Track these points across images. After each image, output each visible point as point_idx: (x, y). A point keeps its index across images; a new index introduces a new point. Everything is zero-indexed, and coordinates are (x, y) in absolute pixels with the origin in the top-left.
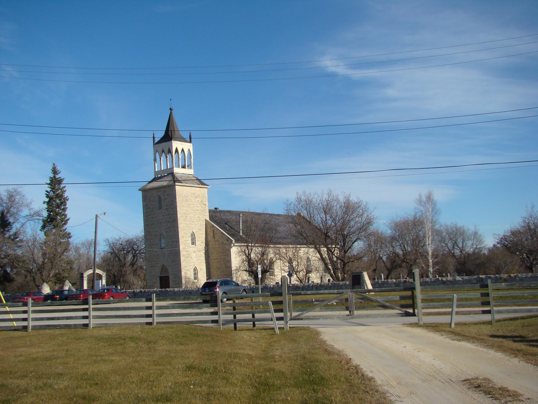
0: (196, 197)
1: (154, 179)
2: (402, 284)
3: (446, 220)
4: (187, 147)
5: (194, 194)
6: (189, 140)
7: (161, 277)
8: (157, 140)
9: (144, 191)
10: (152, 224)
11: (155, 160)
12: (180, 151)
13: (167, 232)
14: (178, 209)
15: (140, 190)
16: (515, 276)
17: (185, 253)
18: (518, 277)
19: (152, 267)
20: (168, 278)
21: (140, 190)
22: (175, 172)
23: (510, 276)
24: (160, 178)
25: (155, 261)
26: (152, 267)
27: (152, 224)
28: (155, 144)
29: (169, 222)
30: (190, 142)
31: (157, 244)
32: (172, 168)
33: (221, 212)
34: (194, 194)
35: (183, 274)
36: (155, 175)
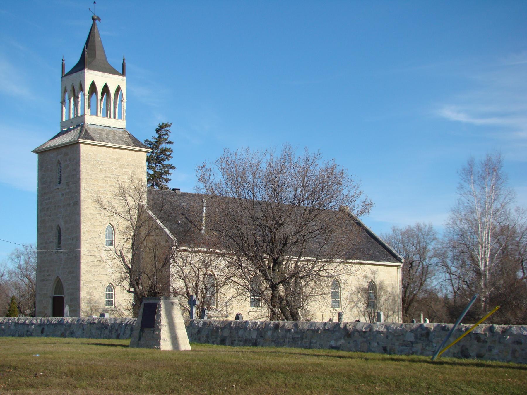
0: (122, 166)
1: (60, 133)
2: (269, 333)
3: (299, 157)
4: (114, 81)
5: (118, 160)
6: (121, 72)
7: (54, 298)
8: (67, 70)
9: (41, 152)
10: (48, 209)
11: (63, 103)
12: (100, 89)
13: (66, 222)
14: (83, 184)
15: (34, 152)
16: (504, 331)
17: (90, 259)
18: (511, 334)
19: (43, 280)
20: (62, 299)
21: (34, 152)
22: (86, 122)
23: (491, 329)
24: (66, 132)
25: (48, 271)
26: (43, 280)
27: (48, 209)
28: (65, 76)
29: (69, 204)
30: (123, 74)
31: (52, 242)
32: (83, 116)
33: (184, 195)
34: (118, 160)
35: (83, 294)
36: (62, 127)
